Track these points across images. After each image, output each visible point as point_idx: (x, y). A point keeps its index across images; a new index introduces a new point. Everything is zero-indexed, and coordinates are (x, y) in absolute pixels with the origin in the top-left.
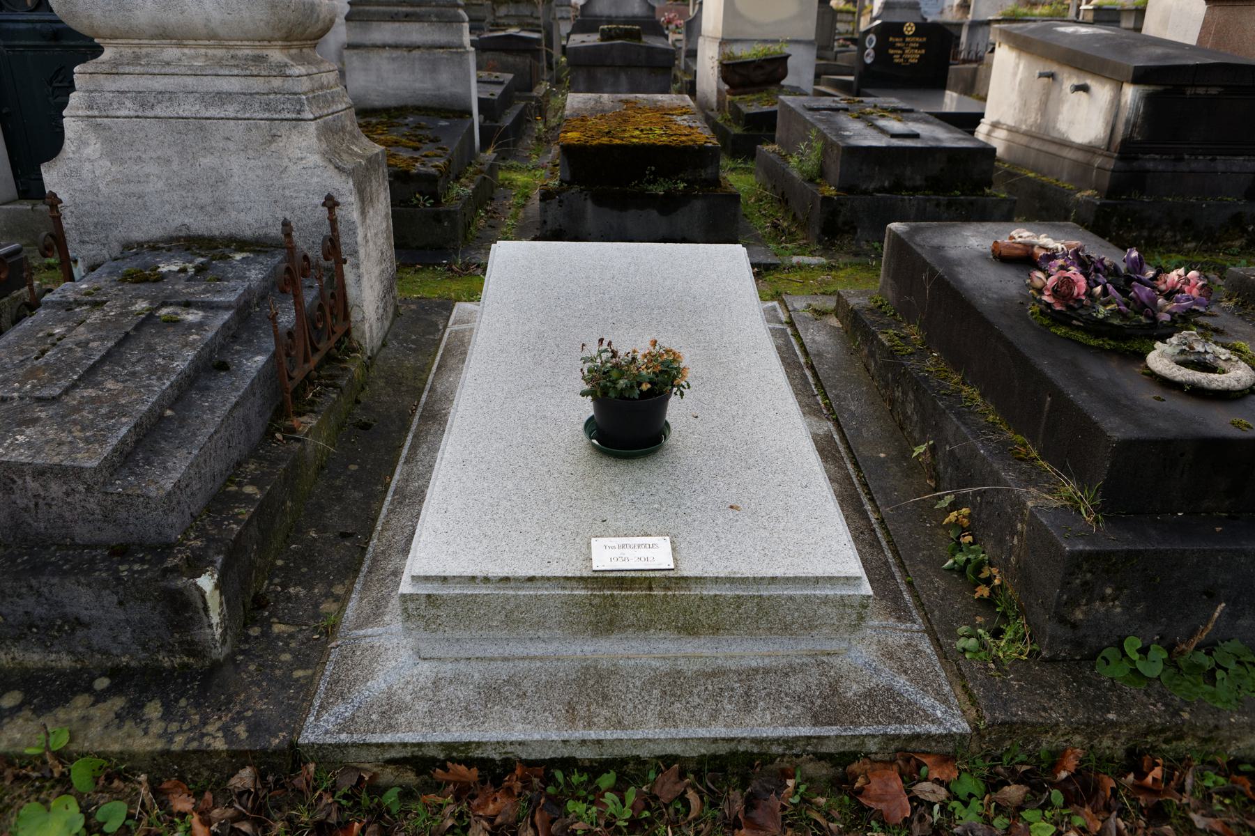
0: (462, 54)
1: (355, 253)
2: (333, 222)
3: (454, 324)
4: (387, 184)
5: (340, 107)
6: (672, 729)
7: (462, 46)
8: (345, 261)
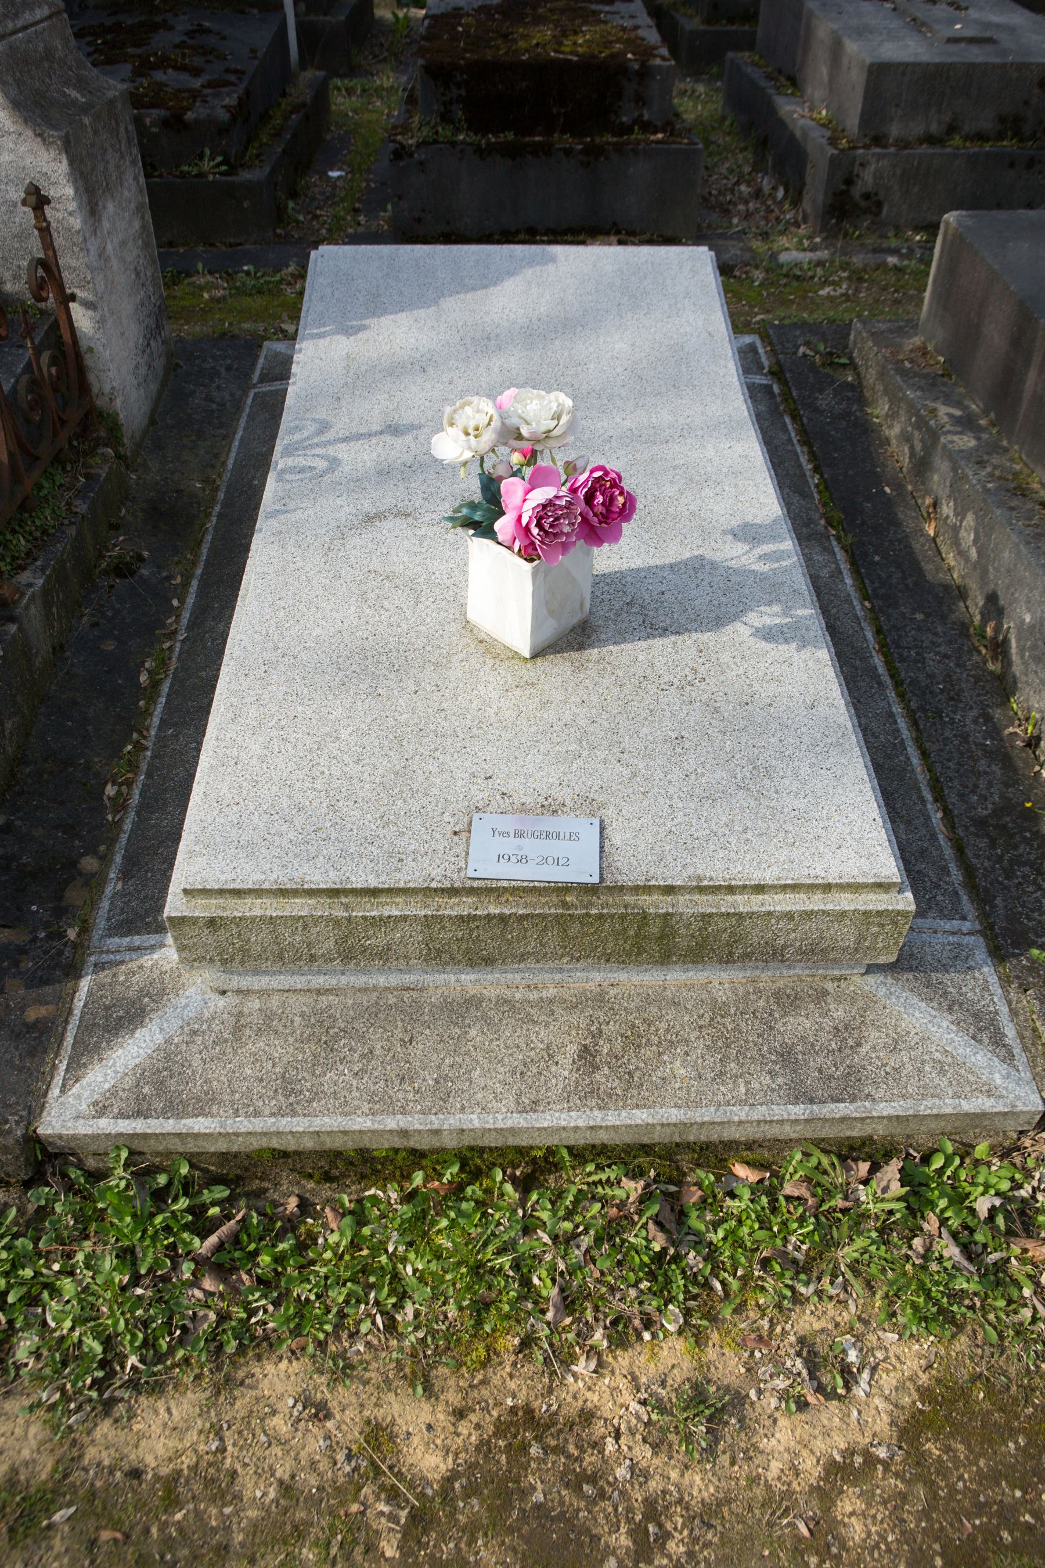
2: (45, 231)
3: (263, 379)
4: (135, 151)
6: (596, 1112)
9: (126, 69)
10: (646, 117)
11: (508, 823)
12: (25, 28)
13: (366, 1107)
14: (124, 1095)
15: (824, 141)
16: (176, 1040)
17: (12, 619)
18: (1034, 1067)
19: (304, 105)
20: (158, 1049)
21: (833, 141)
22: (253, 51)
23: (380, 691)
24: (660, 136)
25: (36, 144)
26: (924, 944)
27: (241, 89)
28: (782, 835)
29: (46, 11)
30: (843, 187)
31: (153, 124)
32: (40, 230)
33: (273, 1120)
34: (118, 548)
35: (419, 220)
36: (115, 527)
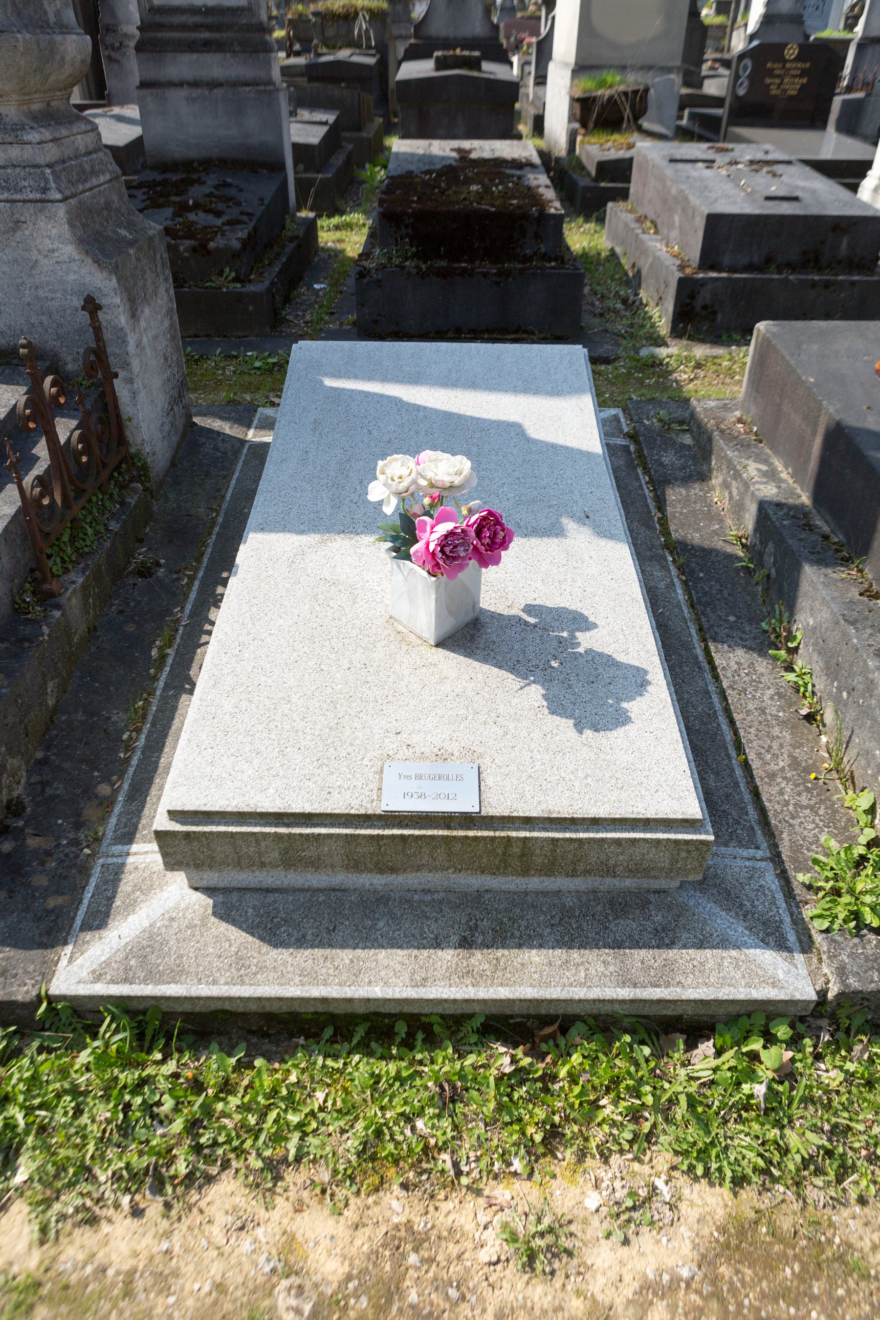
0: (270, 93)
1: (126, 365)
2: (97, 330)
4: (168, 272)
5: (102, 179)
6: (470, 988)
7: (270, 82)
8: (116, 375)
9: (169, 212)
10: (543, 250)
11: (412, 768)
12: (91, 189)
13: (297, 979)
14: (115, 966)
15: (675, 268)
16: (158, 924)
17: (58, 607)
18: (810, 965)
19: (297, 237)
20: (144, 931)
21: (681, 268)
22: (261, 200)
23: (323, 667)
24: (553, 264)
25: (94, 268)
26: (726, 866)
27: (252, 225)
28: (613, 781)
29: (108, 177)
30: (688, 301)
31: (185, 251)
32: (94, 328)
33: (227, 987)
34: (142, 554)
35: (376, 322)
36: (141, 541)
